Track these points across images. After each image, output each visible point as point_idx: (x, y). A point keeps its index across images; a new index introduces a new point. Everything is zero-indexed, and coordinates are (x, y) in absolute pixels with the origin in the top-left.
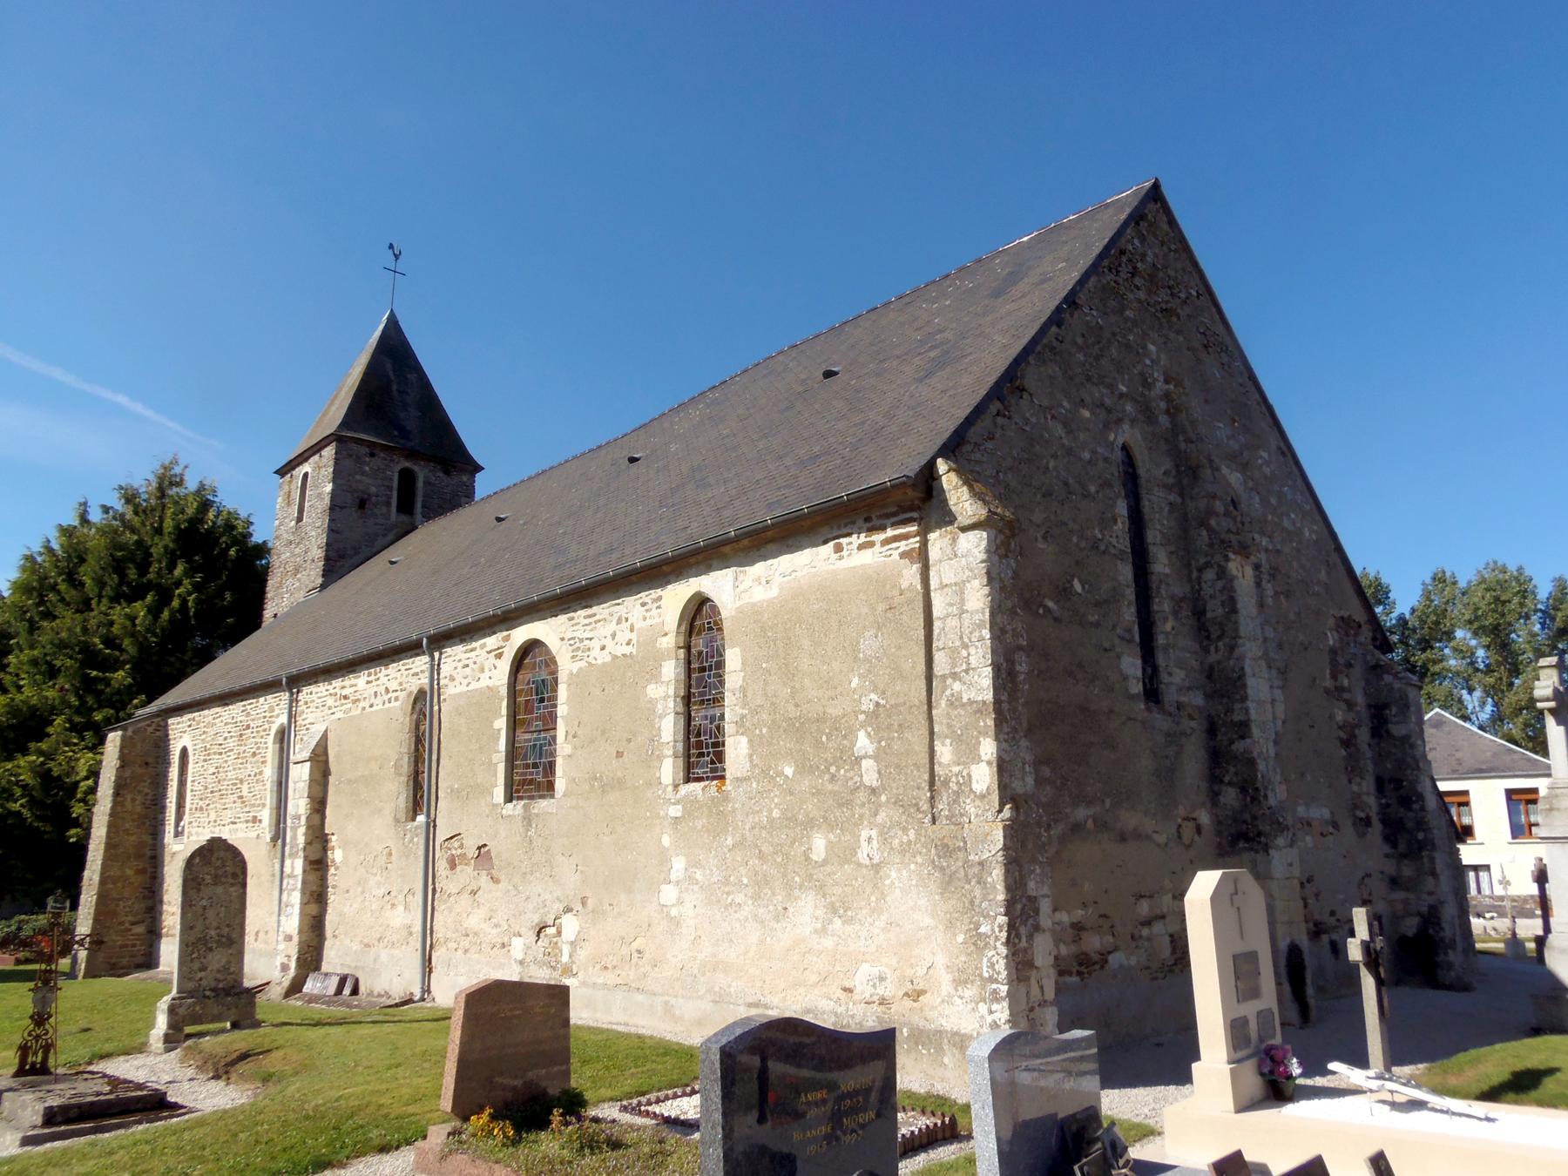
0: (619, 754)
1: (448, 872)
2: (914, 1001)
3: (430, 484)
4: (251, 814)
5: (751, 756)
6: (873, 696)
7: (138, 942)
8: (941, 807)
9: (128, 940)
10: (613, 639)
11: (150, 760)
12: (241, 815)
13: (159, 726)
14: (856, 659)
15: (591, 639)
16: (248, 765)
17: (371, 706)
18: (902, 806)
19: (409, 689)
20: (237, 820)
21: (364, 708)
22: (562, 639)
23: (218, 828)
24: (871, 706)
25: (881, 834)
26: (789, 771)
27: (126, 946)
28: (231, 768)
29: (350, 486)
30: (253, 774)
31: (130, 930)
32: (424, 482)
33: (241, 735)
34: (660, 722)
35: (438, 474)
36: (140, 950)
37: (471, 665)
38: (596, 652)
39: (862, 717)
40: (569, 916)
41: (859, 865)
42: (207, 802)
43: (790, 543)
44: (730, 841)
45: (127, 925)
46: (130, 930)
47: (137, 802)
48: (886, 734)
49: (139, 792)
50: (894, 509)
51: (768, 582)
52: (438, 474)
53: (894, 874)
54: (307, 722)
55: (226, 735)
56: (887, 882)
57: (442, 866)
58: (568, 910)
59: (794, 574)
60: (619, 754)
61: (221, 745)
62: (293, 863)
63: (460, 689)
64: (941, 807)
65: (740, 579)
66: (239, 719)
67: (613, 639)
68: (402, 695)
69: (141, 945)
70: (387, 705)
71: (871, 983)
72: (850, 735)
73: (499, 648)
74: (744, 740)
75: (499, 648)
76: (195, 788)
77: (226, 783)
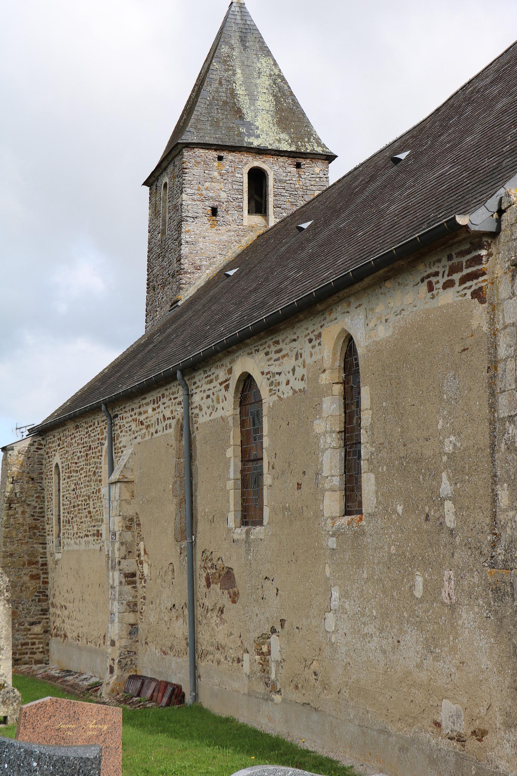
0: (299, 486)
1: (205, 590)
2: (480, 740)
3: (280, 181)
4: (96, 528)
5: (377, 492)
6: (452, 438)
7: (37, 641)
8: (499, 551)
9: (29, 639)
10: (294, 374)
11: (34, 476)
12: (90, 529)
13: (41, 444)
14: (441, 400)
15: (280, 374)
16: (92, 483)
17: (156, 432)
18: (470, 548)
19: (177, 417)
20: (89, 533)
21: (152, 434)
22: (263, 373)
23: (79, 539)
24: (451, 448)
25: (456, 575)
26: (400, 509)
27: (26, 644)
28: (83, 485)
29: (201, 195)
30: (95, 491)
31: (29, 630)
32: (275, 180)
33: (87, 454)
34: (322, 455)
35: (289, 169)
36: (38, 648)
37: (211, 396)
38: (283, 387)
39: (445, 458)
40: (274, 636)
41: (443, 603)
42: (72, 515)
43: (400, 281)
44: (365, 576)
45: (26, 624)
46: (29, 630)
47: (27, 515)
48: (460, 477)
49: (29, 505)
50: (467, 246)
51: (386, 321)
52: (289, 169)
53: (464, 615)
54: (122, 445)
55: (79, 454)
56: (460, 622)
57: (201, 582)
58: (273, 631)
59: (403, 313)
60: (299, 486)
61: (76, 463)
62: (113, 575)
63: (207, 418)
64: (499, 551)
65: (370, 317)
66: (85, 440)
67: (294, 374)
68: (173, 422)
69: (40, 643)
70: (155, 435)
71: (452, 720)
72: (437, 477)
73: (226, 381)
74: (372, 476)
75: (226, 381)
76: (65, 503)
77: (81, 499)
